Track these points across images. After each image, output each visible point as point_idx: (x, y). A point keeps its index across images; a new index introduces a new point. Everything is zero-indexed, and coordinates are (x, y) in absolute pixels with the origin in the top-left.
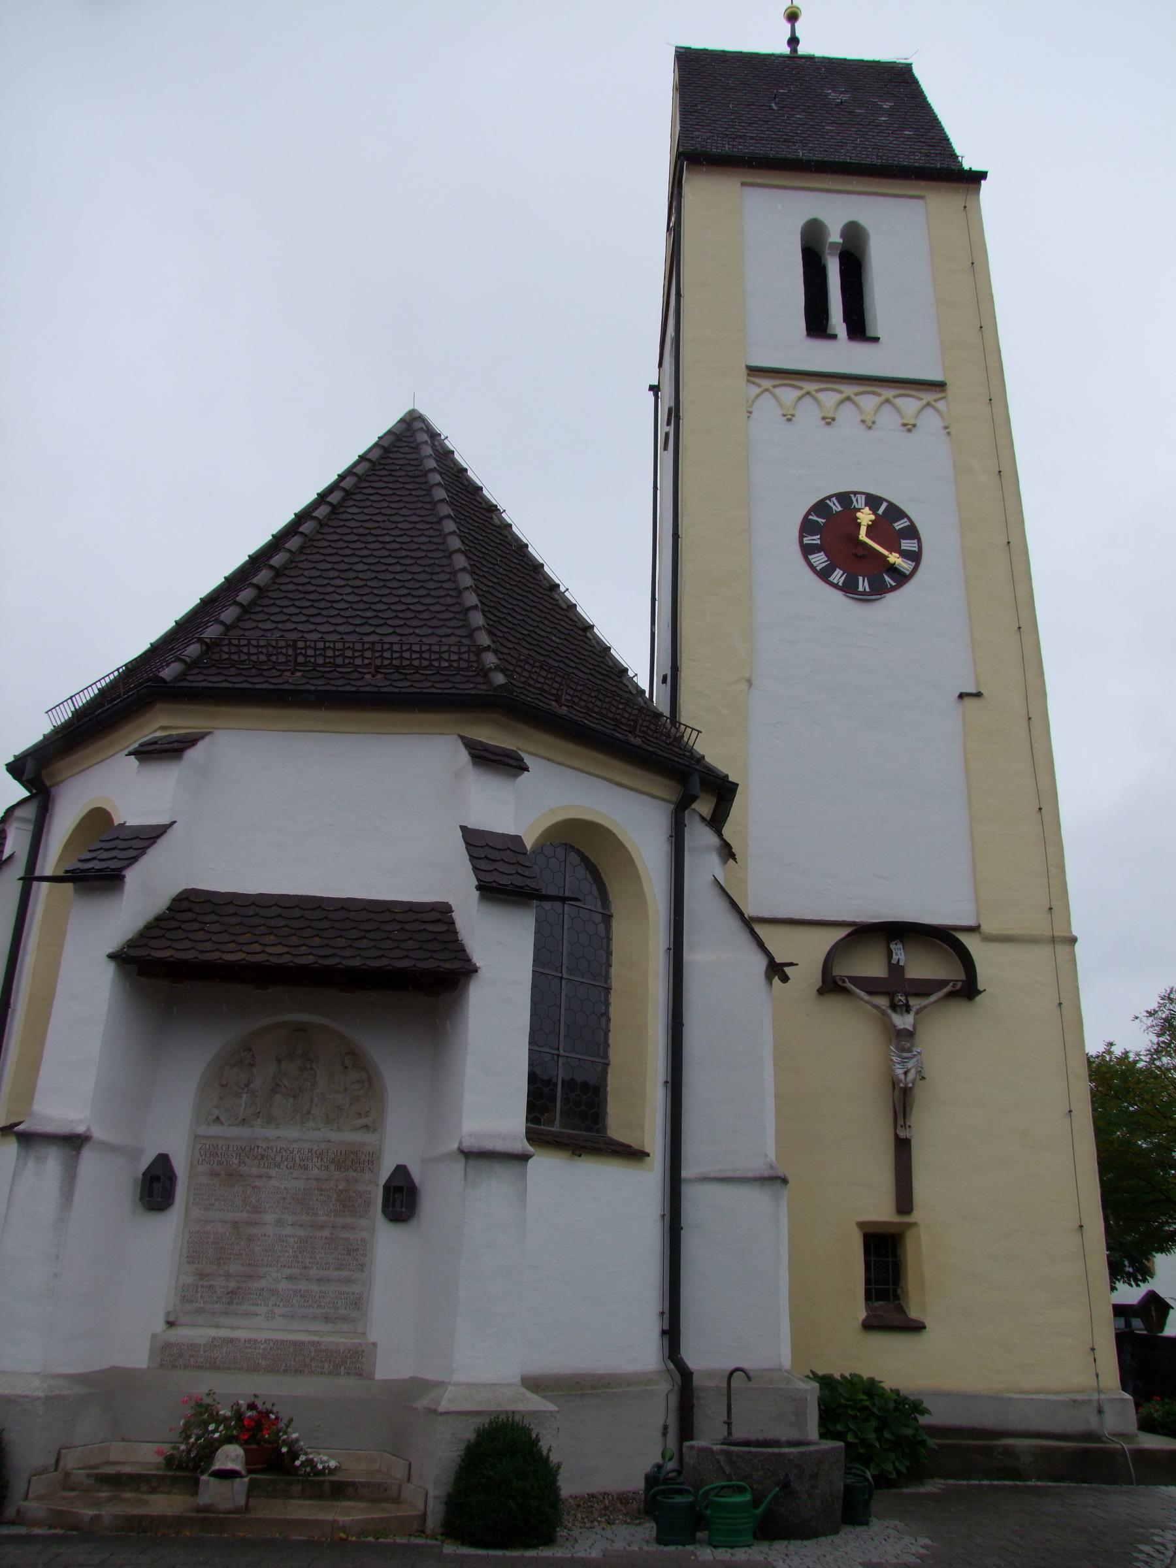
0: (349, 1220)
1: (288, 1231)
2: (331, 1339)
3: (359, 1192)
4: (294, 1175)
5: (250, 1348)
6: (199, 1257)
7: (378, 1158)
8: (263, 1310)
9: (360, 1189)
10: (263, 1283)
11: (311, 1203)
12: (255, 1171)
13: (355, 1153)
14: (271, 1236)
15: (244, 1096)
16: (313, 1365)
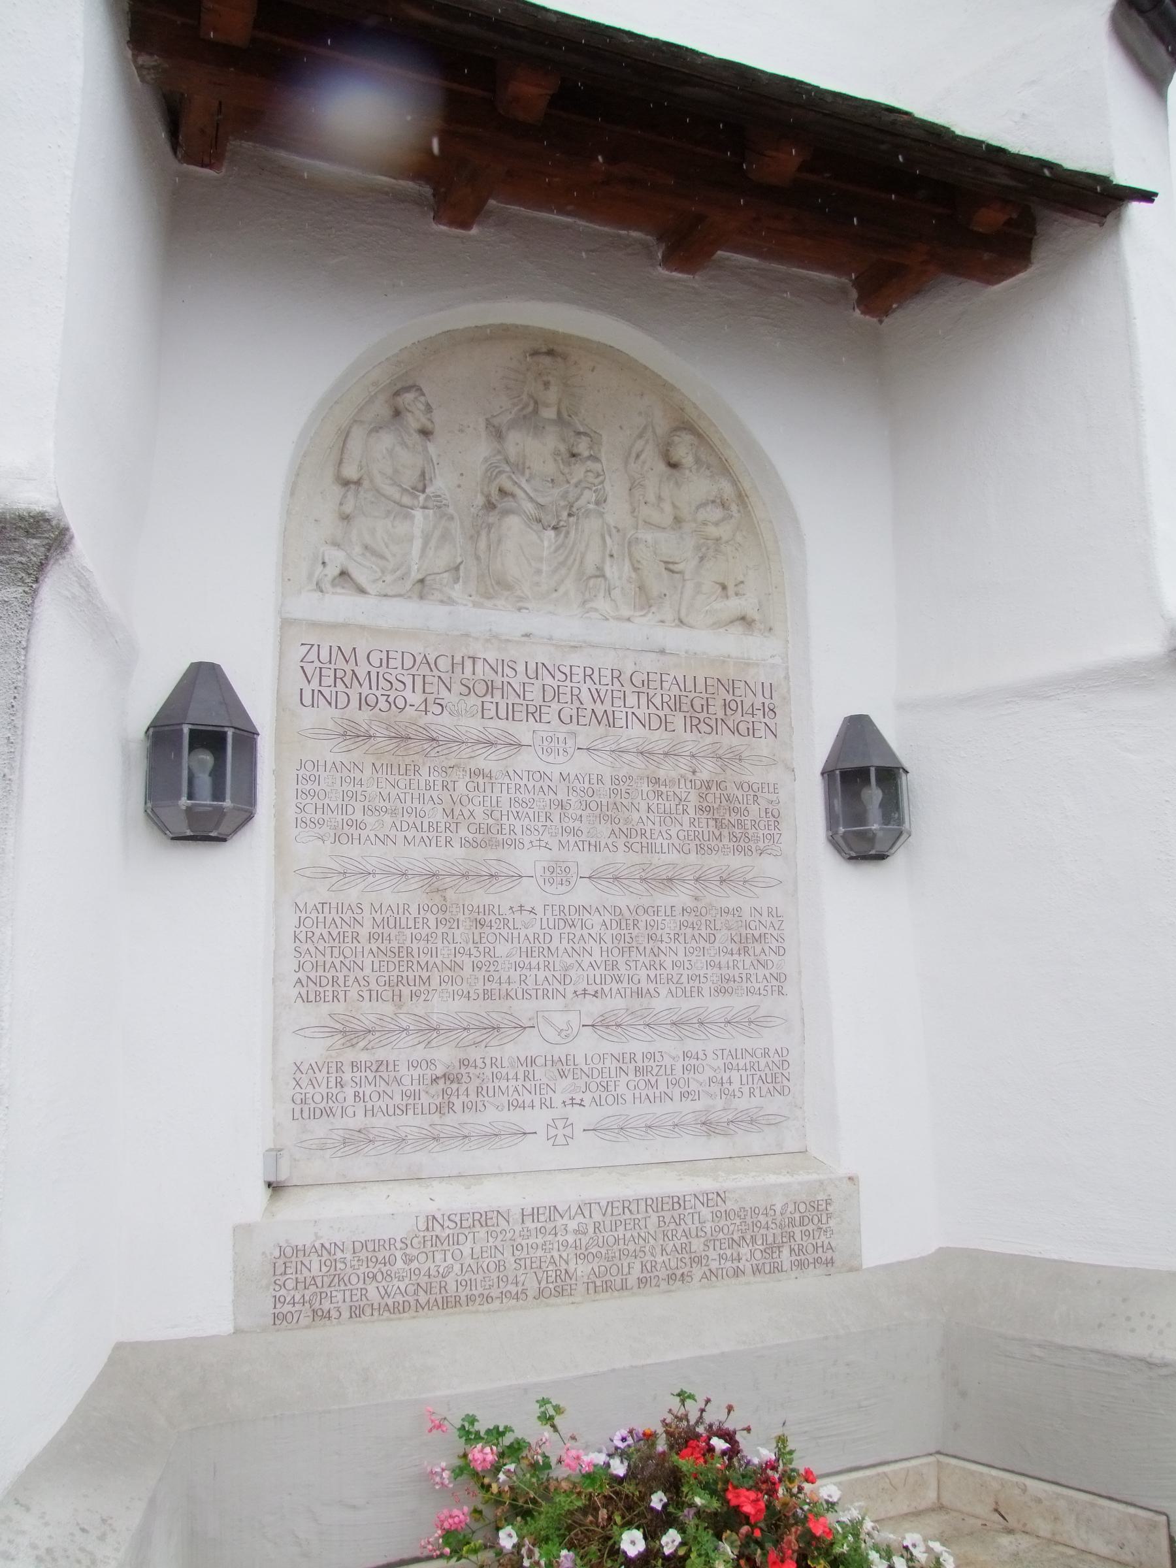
0: (736, 862)
1: (584, 894)
2: (745, 1181)
4: (582, 741)
5: (539, 1231)
6: (334, 981)
8: (537, 1119)
9: (752, 779)
10: (531, 1045)
11: (635, 816)
12: (472, 726)
13: (731, 687)
14: (539, 910)
15: (418, 514)
16: (713, 1254)
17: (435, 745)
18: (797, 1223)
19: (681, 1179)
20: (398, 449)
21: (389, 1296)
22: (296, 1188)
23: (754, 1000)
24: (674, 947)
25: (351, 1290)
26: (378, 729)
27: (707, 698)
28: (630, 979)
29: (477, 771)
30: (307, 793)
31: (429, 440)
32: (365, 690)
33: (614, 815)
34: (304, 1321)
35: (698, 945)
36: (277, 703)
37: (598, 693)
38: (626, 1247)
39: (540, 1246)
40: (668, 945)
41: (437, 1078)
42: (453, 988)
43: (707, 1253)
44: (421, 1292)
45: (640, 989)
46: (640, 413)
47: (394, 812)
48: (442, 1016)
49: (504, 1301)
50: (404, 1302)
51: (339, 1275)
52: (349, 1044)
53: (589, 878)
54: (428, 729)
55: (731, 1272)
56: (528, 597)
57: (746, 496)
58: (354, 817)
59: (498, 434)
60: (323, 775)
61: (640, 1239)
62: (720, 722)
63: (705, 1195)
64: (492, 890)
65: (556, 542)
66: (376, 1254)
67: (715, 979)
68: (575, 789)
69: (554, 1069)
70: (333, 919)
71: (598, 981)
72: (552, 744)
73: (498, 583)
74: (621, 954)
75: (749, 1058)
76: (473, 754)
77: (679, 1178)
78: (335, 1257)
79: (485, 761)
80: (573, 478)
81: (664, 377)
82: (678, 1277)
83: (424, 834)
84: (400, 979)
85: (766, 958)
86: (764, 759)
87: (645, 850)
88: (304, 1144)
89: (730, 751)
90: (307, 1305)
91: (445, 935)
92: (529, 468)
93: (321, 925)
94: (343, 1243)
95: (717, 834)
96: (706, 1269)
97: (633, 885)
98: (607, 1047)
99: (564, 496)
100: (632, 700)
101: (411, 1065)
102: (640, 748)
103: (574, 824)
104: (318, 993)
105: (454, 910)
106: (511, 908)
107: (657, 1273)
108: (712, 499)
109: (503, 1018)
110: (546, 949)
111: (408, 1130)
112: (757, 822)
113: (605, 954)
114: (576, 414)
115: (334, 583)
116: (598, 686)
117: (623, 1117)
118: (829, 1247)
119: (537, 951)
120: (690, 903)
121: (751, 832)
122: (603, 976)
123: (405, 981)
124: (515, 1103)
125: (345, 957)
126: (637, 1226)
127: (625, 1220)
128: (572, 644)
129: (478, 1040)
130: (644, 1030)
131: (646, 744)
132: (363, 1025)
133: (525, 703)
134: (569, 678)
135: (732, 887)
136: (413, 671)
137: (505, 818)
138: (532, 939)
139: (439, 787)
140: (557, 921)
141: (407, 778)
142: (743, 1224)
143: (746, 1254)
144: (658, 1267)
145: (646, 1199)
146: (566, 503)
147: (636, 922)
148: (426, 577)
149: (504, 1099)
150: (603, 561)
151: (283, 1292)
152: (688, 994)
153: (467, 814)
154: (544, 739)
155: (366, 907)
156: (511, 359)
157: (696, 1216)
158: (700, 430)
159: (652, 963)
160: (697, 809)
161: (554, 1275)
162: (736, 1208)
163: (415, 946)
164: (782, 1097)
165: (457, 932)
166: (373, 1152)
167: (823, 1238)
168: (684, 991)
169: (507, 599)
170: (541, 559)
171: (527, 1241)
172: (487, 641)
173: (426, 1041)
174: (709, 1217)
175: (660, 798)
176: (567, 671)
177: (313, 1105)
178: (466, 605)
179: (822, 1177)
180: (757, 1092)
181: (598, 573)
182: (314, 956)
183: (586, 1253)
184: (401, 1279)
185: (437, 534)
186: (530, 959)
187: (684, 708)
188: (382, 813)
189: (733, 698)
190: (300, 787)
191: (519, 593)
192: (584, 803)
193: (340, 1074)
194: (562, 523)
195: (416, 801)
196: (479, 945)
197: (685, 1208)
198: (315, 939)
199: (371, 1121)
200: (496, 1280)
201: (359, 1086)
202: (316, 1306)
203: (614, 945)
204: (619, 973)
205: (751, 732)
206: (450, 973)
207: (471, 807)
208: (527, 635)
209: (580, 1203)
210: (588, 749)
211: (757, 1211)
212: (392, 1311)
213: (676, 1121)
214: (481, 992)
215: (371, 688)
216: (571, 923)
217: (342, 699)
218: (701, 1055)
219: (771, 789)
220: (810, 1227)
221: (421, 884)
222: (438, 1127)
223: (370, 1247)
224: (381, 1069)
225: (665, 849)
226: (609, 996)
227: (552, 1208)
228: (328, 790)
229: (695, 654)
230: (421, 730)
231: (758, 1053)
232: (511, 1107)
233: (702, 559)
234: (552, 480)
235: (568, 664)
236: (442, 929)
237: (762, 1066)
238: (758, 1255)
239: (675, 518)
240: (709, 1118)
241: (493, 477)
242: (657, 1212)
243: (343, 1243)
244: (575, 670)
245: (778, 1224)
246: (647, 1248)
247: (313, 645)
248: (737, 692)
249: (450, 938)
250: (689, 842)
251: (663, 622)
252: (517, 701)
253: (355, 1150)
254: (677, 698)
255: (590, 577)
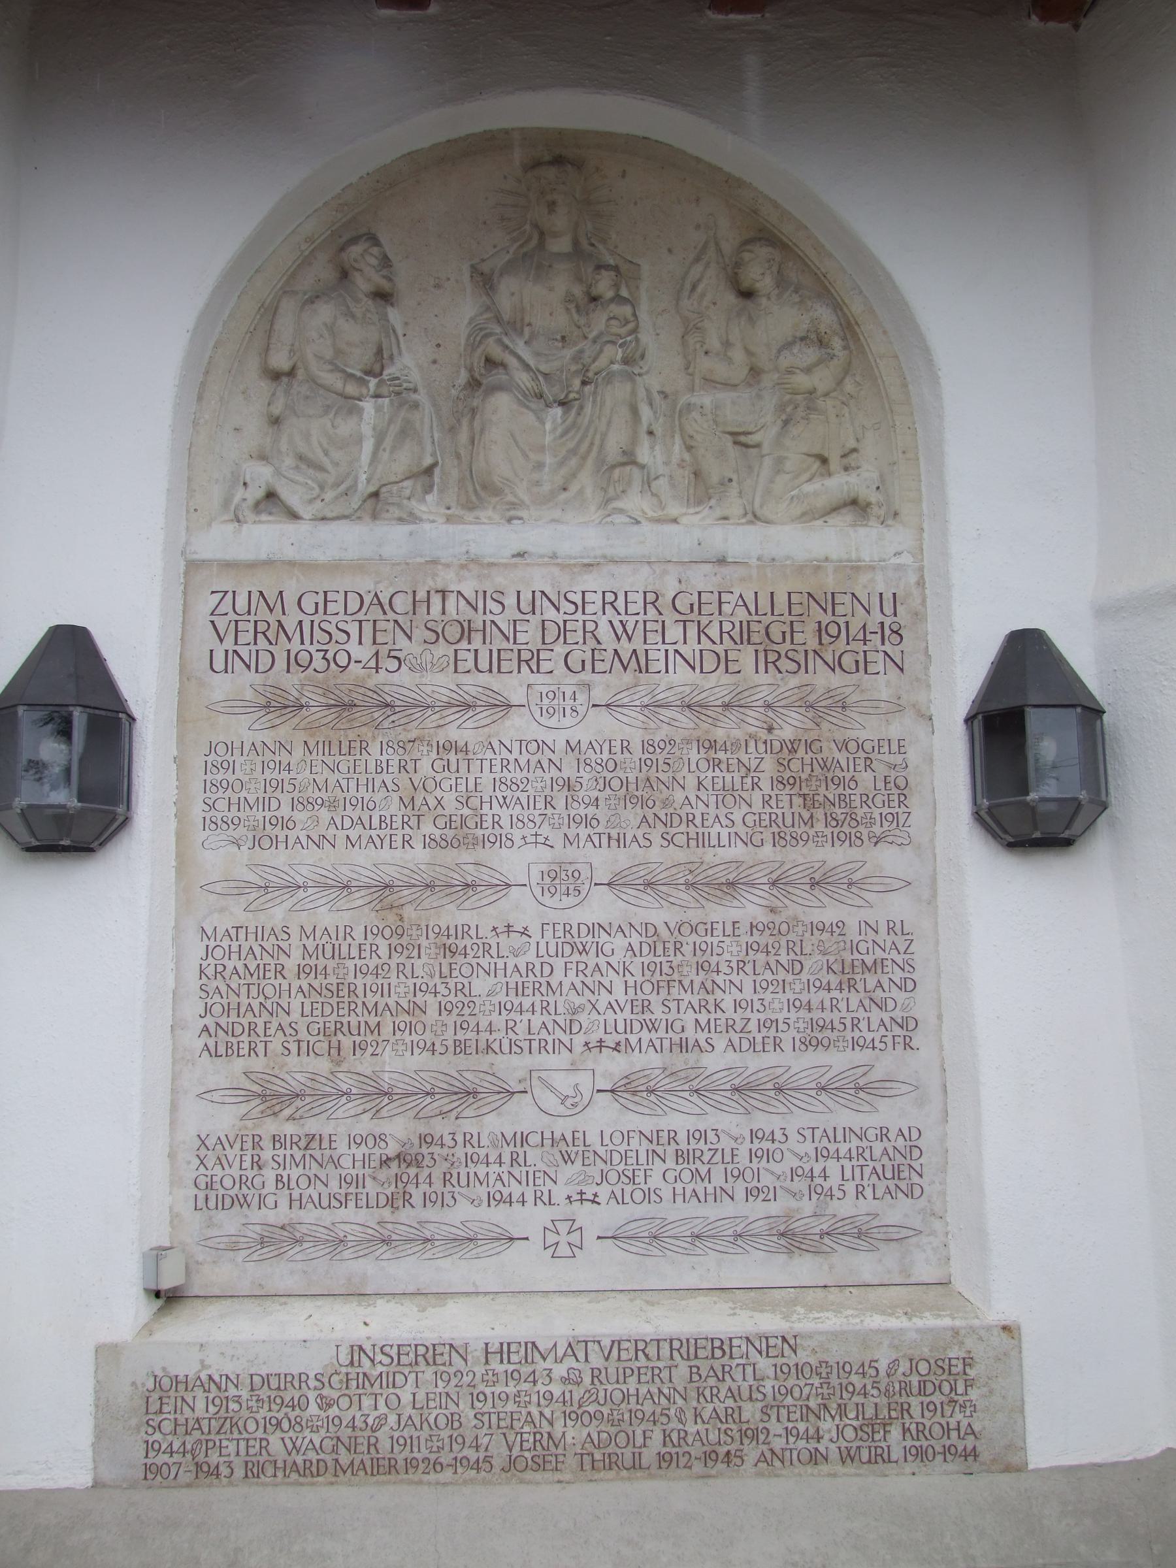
0: (836, 856)
2: (831, 1322)
3: (860, 747)
6: (252, 1028)
7: (918, 616)
9: (862, 735)
11: (679, 796)
12: (441, 684)
13: (831, 602)
14: (535, 931)
15: (368, 406)
16: (775, 1427)
17: (390, 713)
18: (915, 1390)
19: (735, 1314)
20: (341, 322)
21: (298, 1452)
22: (196, 1300)
23: (862, 1057)
24: (736, 980)
25: (248, 1440)
26: (313, 697)
27: (792, 622)
28: (669, 1026)
29: (447, 744)
30: (218, 785)
31: (392, 305)
32: (295, 646)
33: (646, 796)
34: (184, 1478)
35: (775, 977)
36: (181, 671)
37: (624, 626)
38: (639, 1407)
39: (511, 1397)
40: (727, 978)
41: (388, 1159)
42: (412, 1038)
43: (767, 1425)
44: (342, 1450)
45: (684, 1040)
46: (698, 227)
47: (332, 805)
48: (395, 1076)
49: (460, 1470)
50: (318, 1461)
51: (231, 1418)
52: (271, 1112)
53: (608, 884)
54: (380, 693)
55: (805, 1456)
56: (523, 502)
57: (857, 323)
58: (278, 814)
59: (485, 281)
60: (240, 760)
61: (662, 1398)
62: (811, 655)
63: (764, 1340)
64: (467, 905)
65: (564, 422)
66: (281, 1393)
67: (801, 1025)
68: (588, 761)
69: (556, 1151)
70: (251, 948)
71: (621, 1028)
72: (556, 701)
73: (484, 487)
74: (226, 1013)
75: (855, 1142)
76: (442, 722)
77: (732, 1312)
78: (227, 1394)
79: (460, 730)
80: (590, 332)
81: (727, 168)
82: (721, 1457)
83: (374, 833)
84: (339, 1026)
85: (884, 995)
86: (883, 704)
87: (693, 843)
88: (209, 1243)
89: (827, 696)
90: (189, 1456)
91: (401, 967)
92: (529, 324)
93: (234, 956)
94: (238, 1375)
95: (806, 815)
96: (765, 1448)
97: (674, 892)
98: (634, 1121)
99: (577, 358)
100: (674, 633)
101: (353, 1141)
102: (687, 700)
103: (586, 811)
104: (230, 1045)
105: (414, 933)
106: (495, 929)
107: (687, 1449)
108: (803, 334)
109: (481, 1080)
110: (545, 985)
111: (347, 1228)
112: (871, 797)
113: (631, 991)
114: (604, 241)
115: (257, 507)
116: (624, 618)
117: (658, 1221)
118: (969, 1431)
119: (531, 987)
120: (762, 917)
121: (860, 812)
122: (628, 1022)
123: (345, 1029)
124: (498, 1197)
125: (266, 998)
126: (656, 1378)
127: (639, 1369)
128: (586, 561)
129: (445, 1109)
130: (690, 1098)
131: (695, 693)
132: (289, 1087)
133: (515, 648)
134: (580, 609)
135: (829, 893)
136: (360, 616)
137: (486, 806)
138: (523, 972)
139: (394, 768)
140: (560, 945)
141: (351, 758)
142: (825, 1386)
143: (829, 1431)
144: (690, 1439)
145: (671, 1341)
146: (580, 367)
147: (678, 946)
148: (380, 488)
149: (482, 1191)
150: (634, 441)
151: (158, 1436)
152: (759, 1047)
153: (432, 802)
154: (544, 695)
155: (295, 931)
156: (505, 177)
157: (749, 1370)
158: (783, 238)
159: (703, 1003)
160: (775, 783)
161: (532, 1440)
162: (813, 1361)
163: (359, 982)
164: (910, 1200)
165: (418, 963)
166: (299, 1257)
167: (958, 1416)
168: (752, 1043)
169: (494, 508)
170: (542, 449)
171: (493, 1389)
172: (463, 567)
173: (375, 1109)
174: (771, 1373)
175: (716, 768)
176: (577, 599)
177: (221, 1192)
178: (433, 521)
179: (958, 1323)
180: (868, 1192)
181: (624, 459)
182: (225, 997)
183: (580, 1412)
184: (315, 1429)
185: (394, 429)
186: (520, 998)
187: (755, 638)
188: (317, 807)
189: (833, 618)
190: (209, 777)
191: (510, 498)
192: (601, 781)
193: (257, 1151)
194: (572, 396)
195: (362, 789)
196: (448, 980)
197: (731, 1357)
198: (227, 974)
199: (297, 1214)
200: (447, 1441)
201: (282, 1167)
202: (201, 1458)
203: (647, 978)
204: (653, 1017)
205: (862, 665)
206: (408, 1019)
207: (438, 793)
208: (521, 555)
209: (571, 1340)
210: (608, 706)
211: (847, 1368)
212: (302, 1473)
213: (739, 1229)
214: (450, 1043)
215: (302, 643)
216: (581, 948)
217: (265, 659)
218: (778, 1135)
219: (894, 748)
220: (937, 1398)
221: (368, 899)
222: (389, 1226)
223: (274, 1383)
224: (312, 1145)
225: (724, 840)
226: (637, 1049)
227: (530, 1345)
228: (245, 779)
229: (773, 560)
230: (370, 694)
231: (871, 1134)
232: (493, 1202)
233: (786, 423)
234: (563, 338)
235: (579, 589)
236: (396, 959)
237: (877, 1152)
238: (849, 1433)
239: (751, 369)
240: (791, 1227)
241: (477, 343)
242: (688, 1359)
243: (238, 1375)
244: (589, 597)
245: (883, 1390)
246: (672, 1411)
247: (226, 592)
248: (840, 610)
249: (408, 971)
250: (761, 830)
251: (725, 518)
252: (505, 645)
253: (276, 1253)
254: (745, 624)
255: (613, 467)
